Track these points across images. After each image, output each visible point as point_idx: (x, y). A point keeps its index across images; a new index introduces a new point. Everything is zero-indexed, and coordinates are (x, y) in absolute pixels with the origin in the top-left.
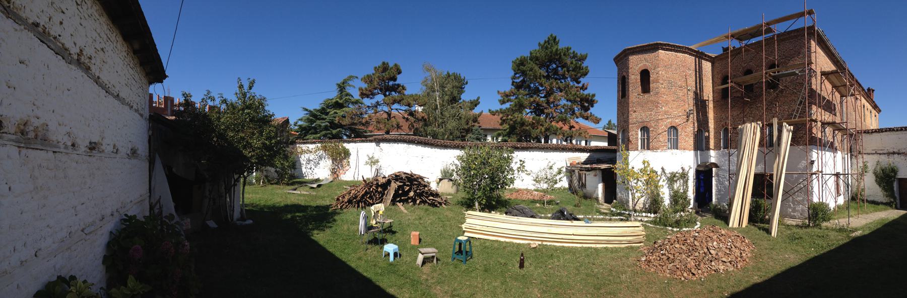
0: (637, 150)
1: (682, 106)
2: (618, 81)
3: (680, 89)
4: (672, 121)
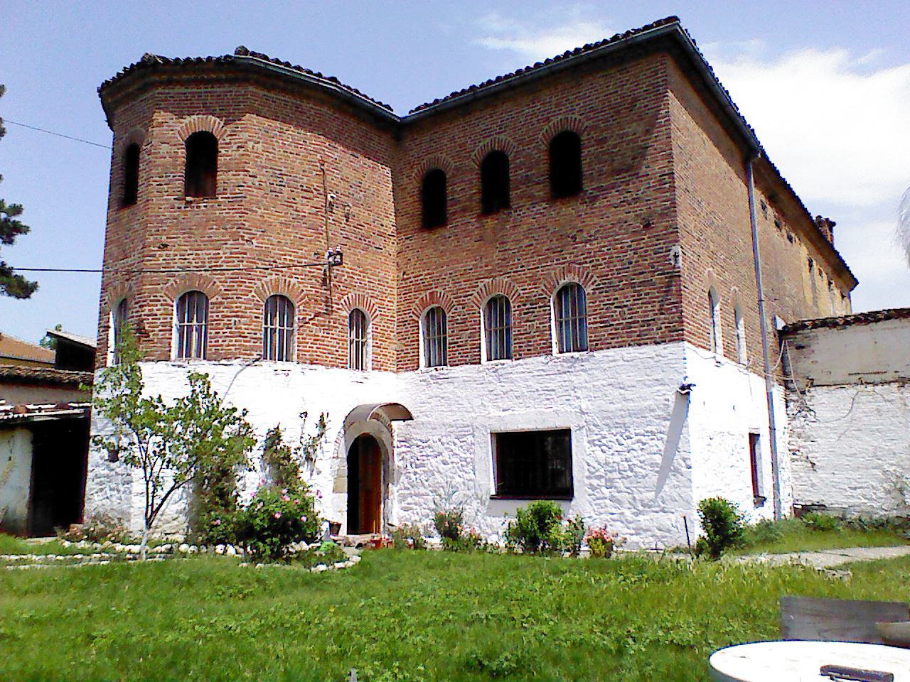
0: (168, 359)
2: (113, 158)
3: (305, 194)
4: (278, 281)
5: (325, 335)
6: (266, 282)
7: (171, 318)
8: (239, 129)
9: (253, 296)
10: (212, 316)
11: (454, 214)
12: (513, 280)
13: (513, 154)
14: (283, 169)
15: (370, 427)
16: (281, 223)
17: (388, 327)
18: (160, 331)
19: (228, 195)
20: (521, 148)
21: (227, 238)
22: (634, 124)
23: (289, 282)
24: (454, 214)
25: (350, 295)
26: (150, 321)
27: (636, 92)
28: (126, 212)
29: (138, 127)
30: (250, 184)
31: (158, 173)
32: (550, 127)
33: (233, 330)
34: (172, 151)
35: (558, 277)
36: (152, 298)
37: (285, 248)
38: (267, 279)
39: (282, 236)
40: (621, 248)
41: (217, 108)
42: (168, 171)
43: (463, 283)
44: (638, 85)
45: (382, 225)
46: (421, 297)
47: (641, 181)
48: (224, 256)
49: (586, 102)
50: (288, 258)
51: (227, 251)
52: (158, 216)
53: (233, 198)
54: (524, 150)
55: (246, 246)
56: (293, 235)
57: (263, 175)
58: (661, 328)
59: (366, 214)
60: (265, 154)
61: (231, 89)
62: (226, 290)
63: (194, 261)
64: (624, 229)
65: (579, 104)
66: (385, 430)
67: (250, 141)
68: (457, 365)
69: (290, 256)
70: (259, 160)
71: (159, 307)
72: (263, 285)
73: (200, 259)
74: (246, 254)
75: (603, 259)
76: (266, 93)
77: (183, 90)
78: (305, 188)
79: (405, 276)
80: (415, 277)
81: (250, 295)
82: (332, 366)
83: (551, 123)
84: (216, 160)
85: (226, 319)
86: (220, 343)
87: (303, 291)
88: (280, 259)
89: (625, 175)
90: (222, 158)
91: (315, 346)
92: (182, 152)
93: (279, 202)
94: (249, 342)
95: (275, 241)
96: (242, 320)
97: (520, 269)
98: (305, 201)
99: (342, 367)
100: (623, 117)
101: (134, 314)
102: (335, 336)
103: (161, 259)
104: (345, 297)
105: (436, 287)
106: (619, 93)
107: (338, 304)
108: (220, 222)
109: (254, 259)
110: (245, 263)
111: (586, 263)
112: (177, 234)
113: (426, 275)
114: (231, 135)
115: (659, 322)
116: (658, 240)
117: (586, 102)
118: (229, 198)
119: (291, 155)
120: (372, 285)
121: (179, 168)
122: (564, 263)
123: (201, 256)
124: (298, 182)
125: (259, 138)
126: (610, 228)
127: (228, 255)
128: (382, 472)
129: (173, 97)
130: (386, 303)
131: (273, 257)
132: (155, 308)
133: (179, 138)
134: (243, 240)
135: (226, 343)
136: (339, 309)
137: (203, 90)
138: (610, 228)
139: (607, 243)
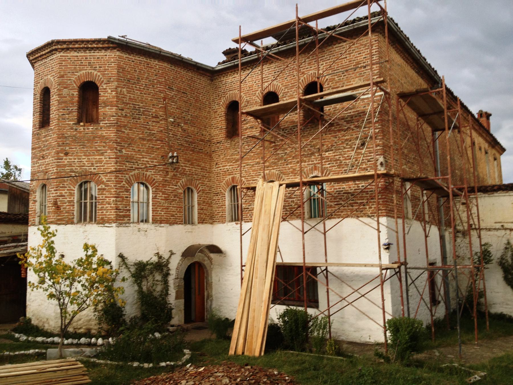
1: (158, 149)
3: (154, 120)
5: (169, 205)
6: (132, 176)
7: (74, 198)
8: (112, 80)
9: (124, 184)
10: (99, 197)
11: (246, 129)
12: (282, 173)
13: (281, 94)
14: (140, 104)
15: (198, 257)
16: (140, 138)
17: (207, 197)
18: (68, 206)
19: (107, 122)
20: (286, 90)
21: (107, 148)
22: (357, 79)
23: (146, 174)
24: (246, 129)
25: (183, 180)
26: (61, 199)
27: (358, 58)
28: (43, 130)
29: (49, 77)
30: (120, 115)
31: (62, 107)
32: (304, 78)
33: (112, 205)
34: (71, 93)
35: (309, 172)
36: (61, 185)
37: (143, 154)
38: (133, 173)
39: (141, 146)
40: (347, 156)
41: (98, 66)
42: (68, 105)
43: (252, 173)
44: (360, 53)
45: (202, 135)
46: (227, 179)
47: (360, 116)
48: (105, 160)
49: (327, 63)
50: (145, 159)
51: (107, 157)
52: (63, 134)
53: (109, 123)
54: (288, 92)
55: (119, 154)
56: (148, 145)
57: (128, 109)
58: (371, 208)
59: (193, 129)
60: (129, 95)
61: (105, 54)
62: (107, 181)
63: (86, 163)
64: (349, 145)
65: (323, 64)
66: (206, 258)
67: (119, 87)
68: (248, 222)
69: (146, 158)
70: (125, 99)
71: (66, 191)
72: (130, 178)
73: (90, 161)
74: (118, 158)
75: (336, 163)
76: (127, 56)
77: (76, 54)
78: (154, 115)
79: (217, 166)
80: (223, 167)
81: (122, 183)
82: (174, 224)
83: (305, 76)
84: (98, 99)
85: (107, 199)
86: (105, 213)
87: (154, 179)
88: (140, 161)
89: (350, 111)
90: (102, 98)
91: (163, 213)
92: (76, 93)
93: (138, 125)
94: (122, 212)
95: (137, 149)
96: (118, 199)
97: (285, 166)
98: (154, 124)
99: (180, 224)
100: (350, 74)
101: (51, 195)
102: (175, 206)
103: (66, 161)
104: (181, 181)
105: (235, 174)
106: (348, 58)
107: (176, 186)
108: (102, 137)
109: (124, 161)
110: (118, 164)
111: (326, 165)
112: (75, 146)
113: (229, 166)
114: (106, 84)
115: (371, 204)
116: (370, 153)
117: (327, 63)
118: (106, 123)
119: (145, 95)
120: (197, 172)
121: (75, 104)
122: (312, 164)
123: (91, 160)
124: (150, 112)
125: (124, 85)
126: (340, 144)
127: (108, 159)
128: (205, 283)
129: (70, 59)
130: (205, 182)
131: (136, 160)
132: (63, 192)
133: (75, 85)
134: (117, 150)
135: (108, 213)
136: (177, 189)
137: (88, 54)
138: (340, 144)
139: (338, 153)
